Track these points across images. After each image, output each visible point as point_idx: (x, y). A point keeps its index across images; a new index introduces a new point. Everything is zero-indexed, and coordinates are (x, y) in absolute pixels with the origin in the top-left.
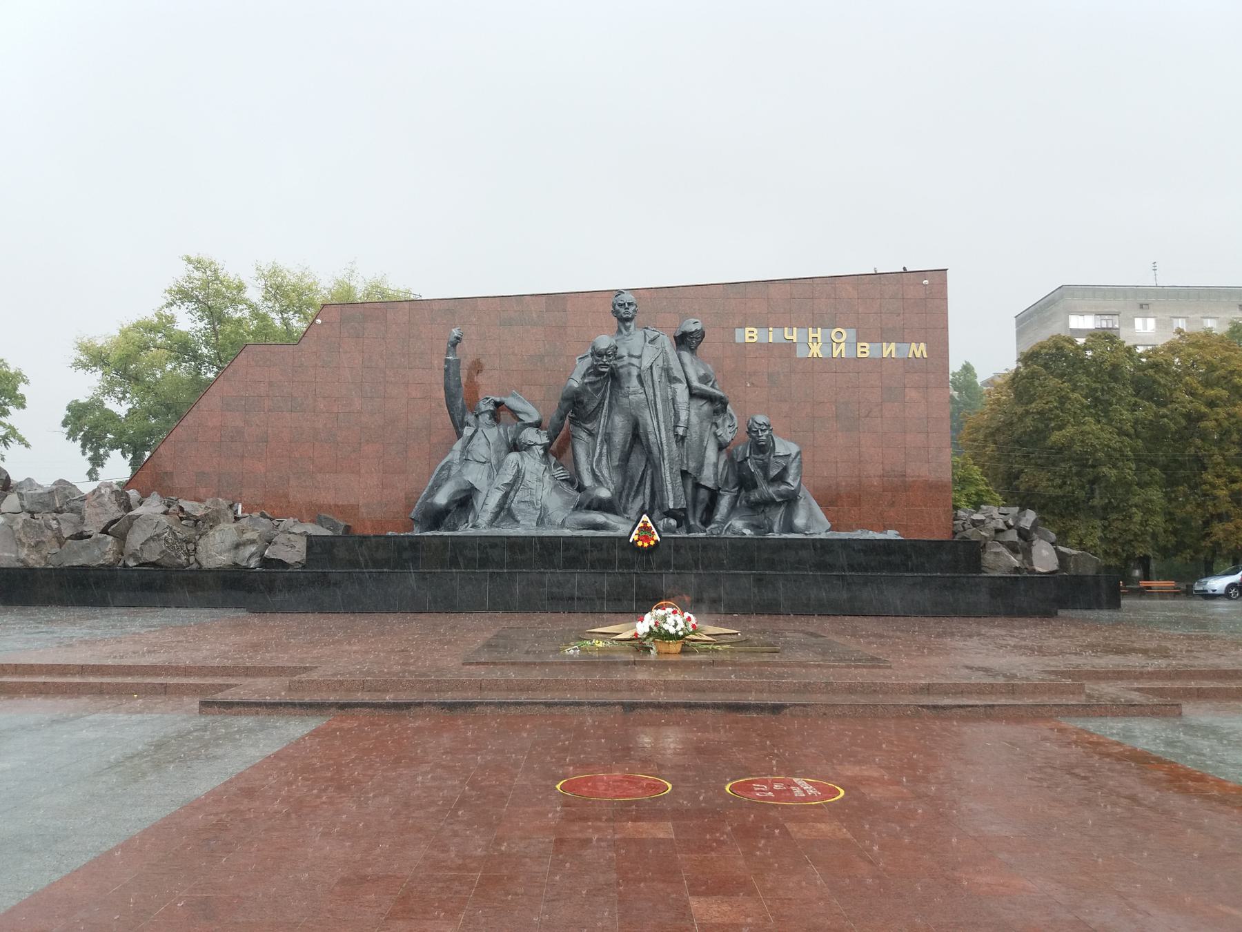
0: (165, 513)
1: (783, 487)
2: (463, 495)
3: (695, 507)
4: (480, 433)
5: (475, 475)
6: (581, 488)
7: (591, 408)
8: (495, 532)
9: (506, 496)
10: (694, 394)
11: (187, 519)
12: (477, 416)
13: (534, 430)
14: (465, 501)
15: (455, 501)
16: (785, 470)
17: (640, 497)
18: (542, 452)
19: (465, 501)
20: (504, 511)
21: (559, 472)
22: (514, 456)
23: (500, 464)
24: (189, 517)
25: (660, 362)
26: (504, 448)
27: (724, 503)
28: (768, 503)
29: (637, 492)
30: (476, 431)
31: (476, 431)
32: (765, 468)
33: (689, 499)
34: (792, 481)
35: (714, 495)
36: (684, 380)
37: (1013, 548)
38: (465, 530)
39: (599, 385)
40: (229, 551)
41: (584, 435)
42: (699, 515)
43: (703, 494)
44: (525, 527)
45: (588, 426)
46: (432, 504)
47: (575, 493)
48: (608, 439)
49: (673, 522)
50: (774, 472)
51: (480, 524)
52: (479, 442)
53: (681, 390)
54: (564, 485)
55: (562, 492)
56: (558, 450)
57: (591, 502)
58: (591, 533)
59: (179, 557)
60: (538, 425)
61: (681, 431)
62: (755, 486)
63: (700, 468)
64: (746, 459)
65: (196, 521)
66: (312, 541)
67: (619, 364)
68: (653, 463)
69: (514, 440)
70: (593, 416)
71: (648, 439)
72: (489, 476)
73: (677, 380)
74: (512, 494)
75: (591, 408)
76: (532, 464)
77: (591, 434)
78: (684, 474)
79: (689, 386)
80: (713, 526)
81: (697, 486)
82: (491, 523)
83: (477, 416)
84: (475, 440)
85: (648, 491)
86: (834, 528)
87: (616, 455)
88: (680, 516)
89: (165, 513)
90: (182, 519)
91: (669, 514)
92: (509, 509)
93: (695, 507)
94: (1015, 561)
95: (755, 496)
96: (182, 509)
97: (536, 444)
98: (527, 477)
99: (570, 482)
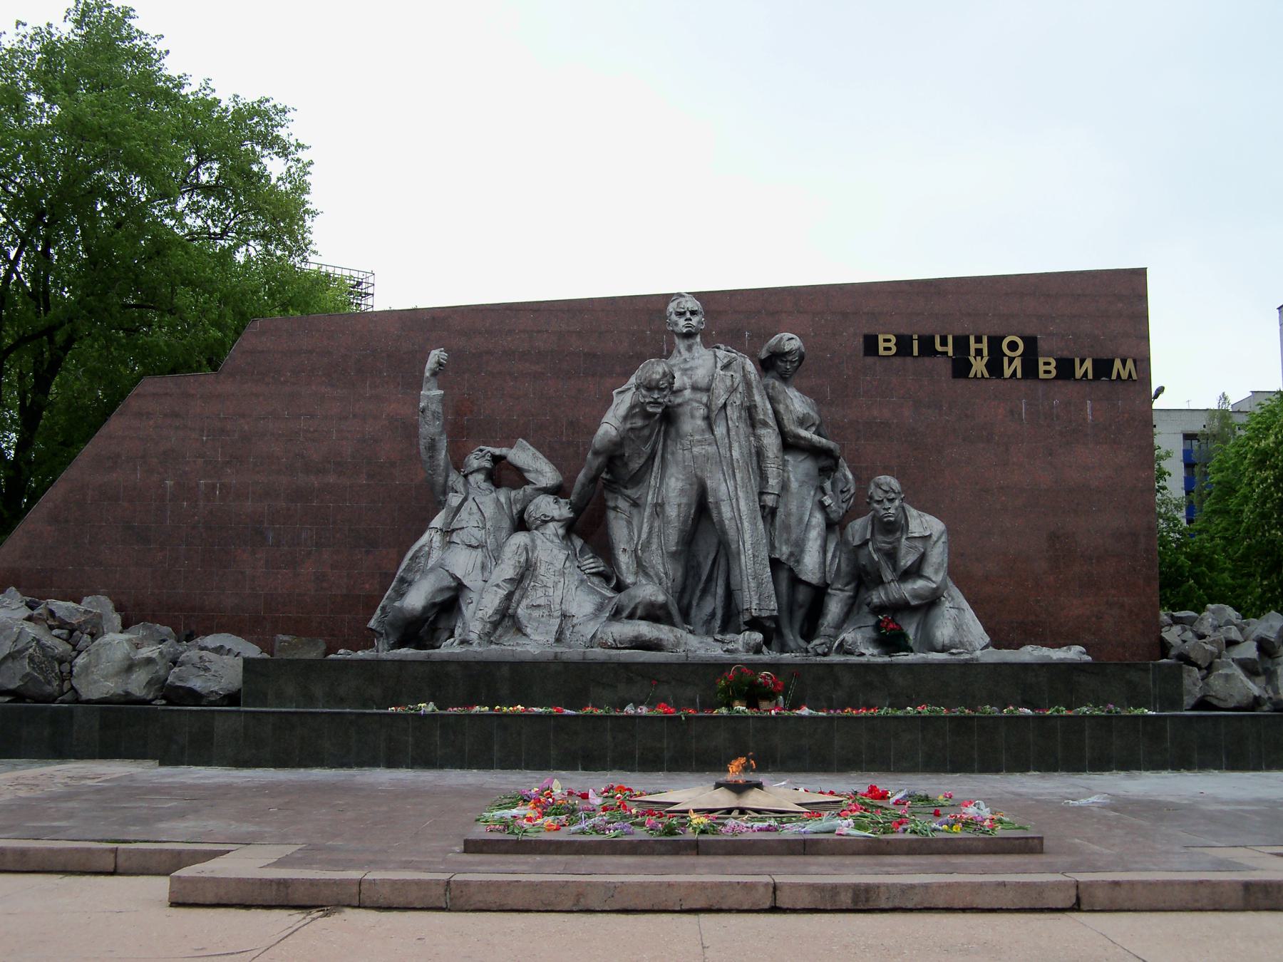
0: (29, 619)
1: (920, 584)
2: (447, 595)
3: (791, 612)
4: (469, 503)
5: (462, 563)
6: (620, 587)
7: (635, 465)
8: (491, 651)
9: (509, 596)
10: (790, 444)
11: (59, 627)
12: (466, 476)
13: (551, 499)
14: (449, 604)
15: (434, 605)
16: (923, 558)
17: (709, 599)
18: (561, 532)
19: (449, 604)
20: (506, 619)
21: (590, 563)
22: (521, 538)
23: (500, 547)
24: (62, 624)
25: (737, 399)
26: (506, 524)
27: (834, 608)
28: (901, 608)
29: (705, 592)
30: (465, 499)
31: (465, 499)
32: (892, 556)
33: (785, 599)
34: (935, 575)
35: (819, 593)
36: (772, 422)
37: (1250, 668)
38: (448, 649)
39: (646, 432)
40: (118, 674)
41: (623, 504)
42: (797, 626)
43: (802, 595)
44: (535, 642)
45: (628, 492)
46: (401, 609)
47: (609, 594)
48: (659, 508)
49: (758, 637)
50: (907, 560)
51: (468, 638)
52: (467, 518)
53: (770, 440)
54: (595, 580)
55: (592, 591)
56: (588, 529)
57: (635, 608)
58: (1232, 807)
59: (49, 683)
60: (557, 491)
61: (770, 500)
62: (880, 582)
63: (797, 555)
64: (865, 543)
65: (72, 632)
66: (249, 664)
67: (679, 400)
68: (725, 551)
69: (522, 512)
70: (638, 479)
71: (720, 513)
72: (483, 567)
73: (765, 424)
74: (517, 596)
75: (635, 465)
76: (549, 549)
77: (635, 504)
78: (775, 564)
79: (783, 433)
80: (817, 642)
81: (795, 581)
82: (487, 637)
83: (466, 476)
84: (464, 513)
85: (720, 591)
86: (998, 641)
87: (673, 536)
88: (771, 631)
89: (29, 619)
90: (51, 628)
91: (755, 624)
92: (514, 617)
93: (791, 612)
94: (1254, 688)
95: (878, 596)
96: (52, 613)
97: (553, 520)
98: (542, 570)
99: (605, 577)
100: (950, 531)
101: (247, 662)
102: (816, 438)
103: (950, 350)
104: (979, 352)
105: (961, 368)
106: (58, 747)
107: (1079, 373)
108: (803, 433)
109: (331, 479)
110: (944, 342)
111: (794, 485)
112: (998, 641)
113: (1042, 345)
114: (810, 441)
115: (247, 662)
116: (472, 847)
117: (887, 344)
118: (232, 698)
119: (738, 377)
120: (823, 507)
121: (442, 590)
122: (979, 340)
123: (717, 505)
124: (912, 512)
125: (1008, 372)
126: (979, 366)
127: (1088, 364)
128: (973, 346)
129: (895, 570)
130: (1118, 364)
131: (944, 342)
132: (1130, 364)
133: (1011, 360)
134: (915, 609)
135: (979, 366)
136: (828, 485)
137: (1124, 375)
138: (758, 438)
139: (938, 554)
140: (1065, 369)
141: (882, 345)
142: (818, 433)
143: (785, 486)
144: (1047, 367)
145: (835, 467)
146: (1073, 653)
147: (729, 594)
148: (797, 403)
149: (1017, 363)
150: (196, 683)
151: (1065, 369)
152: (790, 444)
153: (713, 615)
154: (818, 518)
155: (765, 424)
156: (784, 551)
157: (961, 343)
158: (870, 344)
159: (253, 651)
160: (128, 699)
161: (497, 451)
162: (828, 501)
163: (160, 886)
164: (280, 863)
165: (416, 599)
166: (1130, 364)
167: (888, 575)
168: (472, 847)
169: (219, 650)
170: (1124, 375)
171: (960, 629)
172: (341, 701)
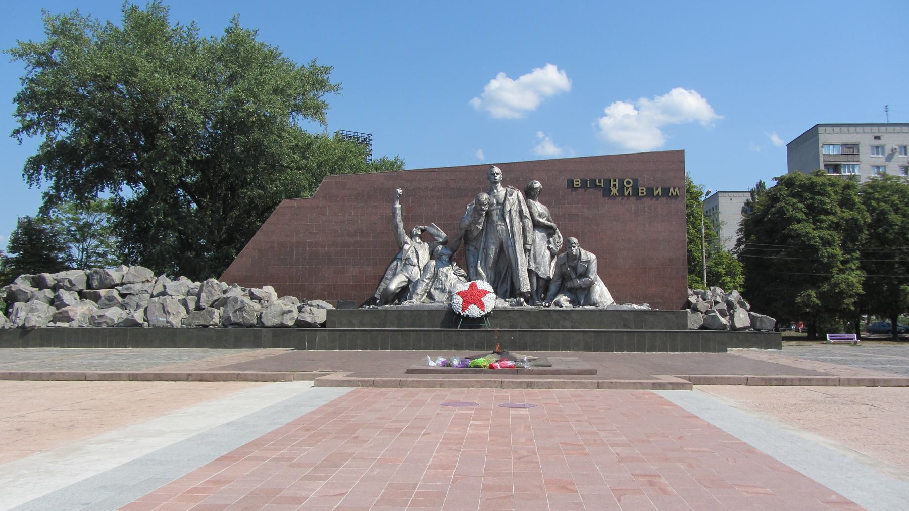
29: (503, 282)
36: (528, 216)
53: (529, 223)
85: (509, 282)
100: (598, 258)
101: (328, 311)
102: (546, 222)
103: (602, 185)
104: (614, 185)
105: (607, 192)
106: (257, 343)
107: (655, 194)
108: (541, 220)
109: (358, 239)
110: (600, 182)
111: (538, 240)
112: (617, 299)
113: (640, 182)
114: (544, 224)
115: (328, 311)
116: (408, 372)
117: (577, 183)
118: (323, 325)
119: (515, 198)
120: (549, 248)
121: (402, 282)
122: (614, 181)
123: (507, 248)
124: (583, 251)
125: (626, 194)
126: (614, 191)
127: (659, 190)
128: (612, 183)
129: (576, 273)
130: (672, 190)
131: (600, 182)
132: (677, 190)
133: (628, 188)
134: (585, 289)
135: (614, 191)
136: (551, 240)
137: (674, 194)
138: (523, 223)
139: (594, 267)
140: (650, 192)
141: (575, 183)
142: (548, 220)
143: (534, 241)
144: (642, 191)
145: (555, 232)
146: (645, 307)
147: (512, 284)
148: (539, 207)
149: (630, 190)
150: (309, 320)
151: (650, 192)
152: (537, 225)
153: (506, 291)
154: (548, 253)
155: (526, 217)
156: (533, 267)
157: (608, 182)
158: (570, 183)
159: (330, 307)
160: (282, 325)
161: (423, 227)
162: (551, 246)
163: (312, 383)
164: (348, 376)
165: (395, 285)
166: (677, 190)
167: (573, 276)
168: (408, 372)
169: (318, 306)
170: (674, 194)
171: (602, 295)
172: (364, 325)
